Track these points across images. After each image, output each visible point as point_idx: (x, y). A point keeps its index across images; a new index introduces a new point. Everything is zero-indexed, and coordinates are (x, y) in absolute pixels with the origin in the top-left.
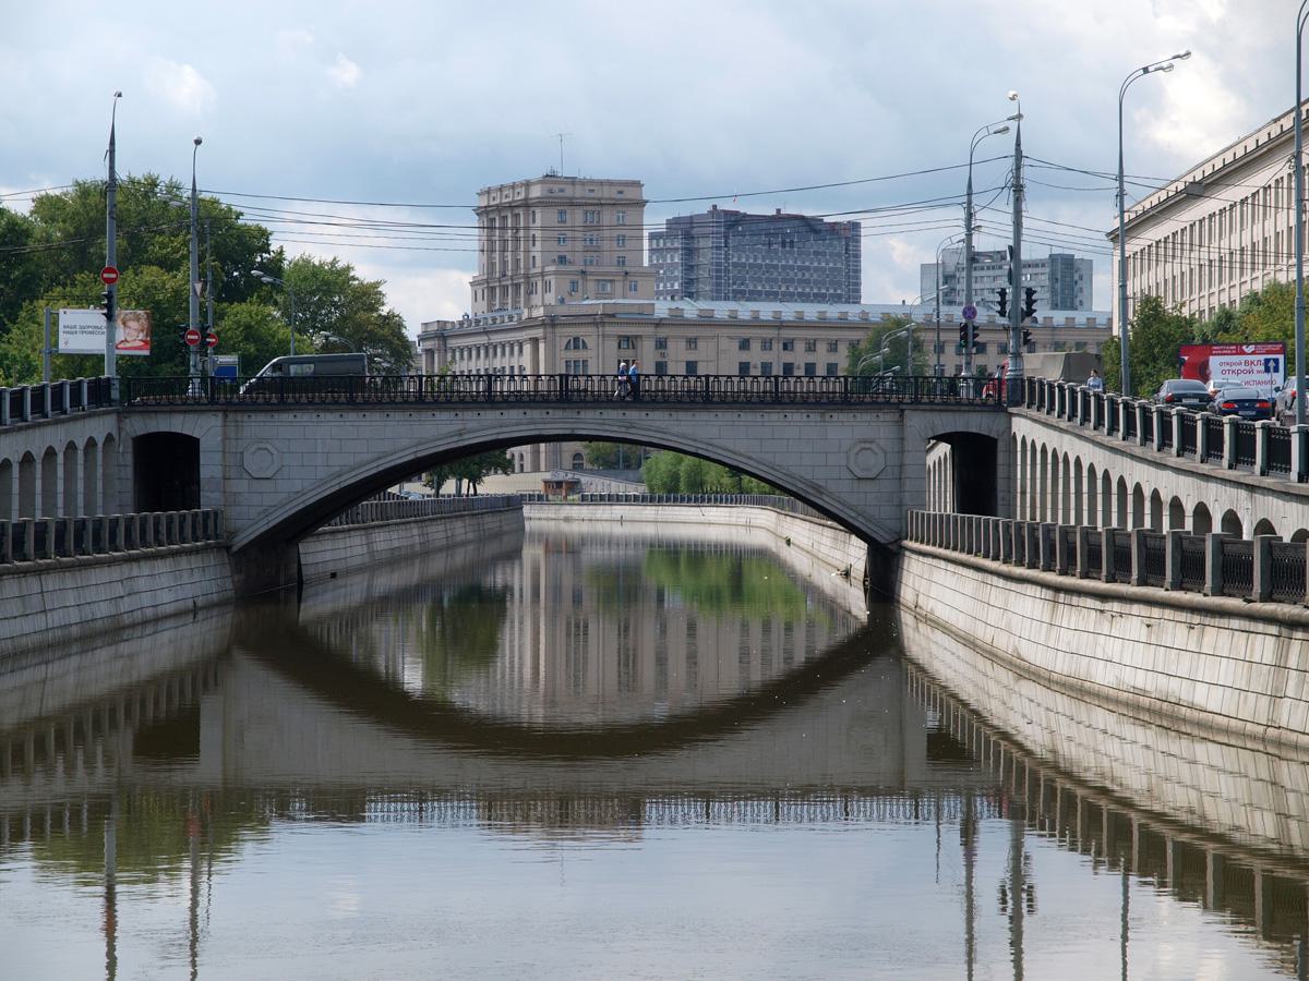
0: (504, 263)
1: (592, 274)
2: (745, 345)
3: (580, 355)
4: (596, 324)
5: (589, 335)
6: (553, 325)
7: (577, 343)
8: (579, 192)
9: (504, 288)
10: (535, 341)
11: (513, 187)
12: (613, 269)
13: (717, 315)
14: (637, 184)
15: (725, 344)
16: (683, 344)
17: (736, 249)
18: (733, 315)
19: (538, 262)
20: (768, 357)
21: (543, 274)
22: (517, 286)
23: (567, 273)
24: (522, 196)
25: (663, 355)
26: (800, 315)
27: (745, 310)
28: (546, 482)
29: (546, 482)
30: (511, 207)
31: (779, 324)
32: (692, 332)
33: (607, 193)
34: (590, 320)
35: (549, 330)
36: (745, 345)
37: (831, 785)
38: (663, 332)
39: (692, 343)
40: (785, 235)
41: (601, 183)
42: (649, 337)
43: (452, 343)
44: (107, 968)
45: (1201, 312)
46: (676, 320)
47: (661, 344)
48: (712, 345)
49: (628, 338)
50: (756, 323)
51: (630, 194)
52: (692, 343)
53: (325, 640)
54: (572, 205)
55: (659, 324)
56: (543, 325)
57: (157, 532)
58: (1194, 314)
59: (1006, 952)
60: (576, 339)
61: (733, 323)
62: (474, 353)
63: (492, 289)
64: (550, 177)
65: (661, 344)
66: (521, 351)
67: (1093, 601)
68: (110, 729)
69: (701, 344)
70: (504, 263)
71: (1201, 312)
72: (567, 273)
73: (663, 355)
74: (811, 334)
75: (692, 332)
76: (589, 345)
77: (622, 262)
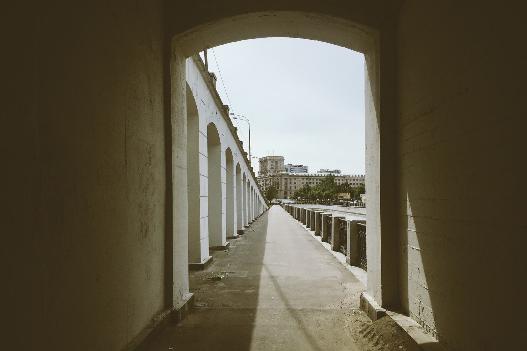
0: (263, 169)
1: (277, 170)
3: (278, 181)
4: (280, 176)
5: (279, 178)
6: (274, 176)
7: (277, 179)
8: (275, 158)
11: (265, 157)
13: (299, 175)
14: (283, 157)
16: (294, 179)
19: (268, 169)
20: (307, 181)
21: (269, 170)
23: (273, 170)
24: (266, 159)
30: (264, 161)
32: (295, 177)
34: (279, 176)
36: (303, 179)
38: (291, 177)
39: (295, 179)
41: (278, 157)
42: (289, 178)
44: (236, 129)
46: (293, 175)
47: (290, 179)
48: (298, 179)
51: (282, 158)
52: (295, 179)
55: (290, 176)
56: (272, 176)
59: (412, 327)
60: (277, 179)
63: (261, 173)
64: (269, 156)
65: (290, 179)
67: (408, 212)
68: (284, 178)
70: (263, 169)
72: (273, 170)
74: (313, 178)
75: (295, 177)
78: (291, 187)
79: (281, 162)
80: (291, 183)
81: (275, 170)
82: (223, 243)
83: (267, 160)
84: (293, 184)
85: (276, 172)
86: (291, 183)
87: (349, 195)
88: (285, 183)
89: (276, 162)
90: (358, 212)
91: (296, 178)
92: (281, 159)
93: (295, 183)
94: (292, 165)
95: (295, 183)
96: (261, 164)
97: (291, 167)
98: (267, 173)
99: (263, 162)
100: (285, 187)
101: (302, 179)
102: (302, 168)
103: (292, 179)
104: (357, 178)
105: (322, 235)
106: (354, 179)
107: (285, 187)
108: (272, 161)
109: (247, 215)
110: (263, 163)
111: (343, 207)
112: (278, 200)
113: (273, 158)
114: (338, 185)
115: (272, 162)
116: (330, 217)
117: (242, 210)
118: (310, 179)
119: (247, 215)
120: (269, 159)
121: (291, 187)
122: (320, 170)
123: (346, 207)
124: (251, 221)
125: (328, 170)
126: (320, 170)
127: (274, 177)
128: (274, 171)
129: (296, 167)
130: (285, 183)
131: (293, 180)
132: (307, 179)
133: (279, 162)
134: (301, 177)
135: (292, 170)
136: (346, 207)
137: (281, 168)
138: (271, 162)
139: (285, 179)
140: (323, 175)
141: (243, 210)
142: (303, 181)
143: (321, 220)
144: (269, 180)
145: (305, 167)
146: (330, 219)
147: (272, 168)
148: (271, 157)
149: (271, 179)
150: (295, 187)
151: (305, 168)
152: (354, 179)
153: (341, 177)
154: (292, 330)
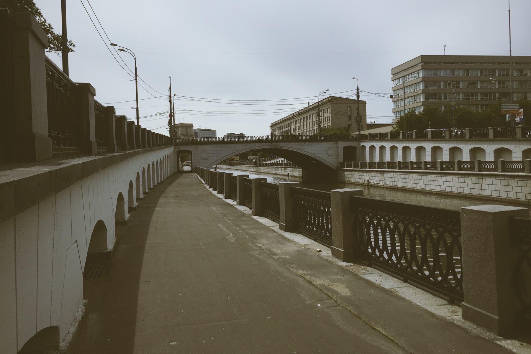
14: (192, 124)
51: (191, 125)
79: (190, 129)
81: (186, 136)
82: (141, 196)
83: (184, 126)
87: (238, 158)
89: (187, 129)
90: (236, 168)
92: (191, 126)
94: (201, 130)
97: (201, 131)
102: (211, 132)
105: (283, 215)
108: (183, 128)
109: (159, 174)
111: (250, 166)
112: (188, 162)
115: (183, 129)
117: (140, 186)
119: (159, 174)
120: (180, 126)
122: (227, 133)
123: (264, 167)
124: (162, 179)
125: (234, 133)
126: (227, 133)
129: (205, 131)
133: (189, 128)
135: (201, 133)
136: (264, 167)
137: (191, 134)
138: (182, 128)
141: (140, 184)
143: (223, 180)
145: (213, 131)
146: (217, 175)
147: (183, 134)
151: (213, 132)
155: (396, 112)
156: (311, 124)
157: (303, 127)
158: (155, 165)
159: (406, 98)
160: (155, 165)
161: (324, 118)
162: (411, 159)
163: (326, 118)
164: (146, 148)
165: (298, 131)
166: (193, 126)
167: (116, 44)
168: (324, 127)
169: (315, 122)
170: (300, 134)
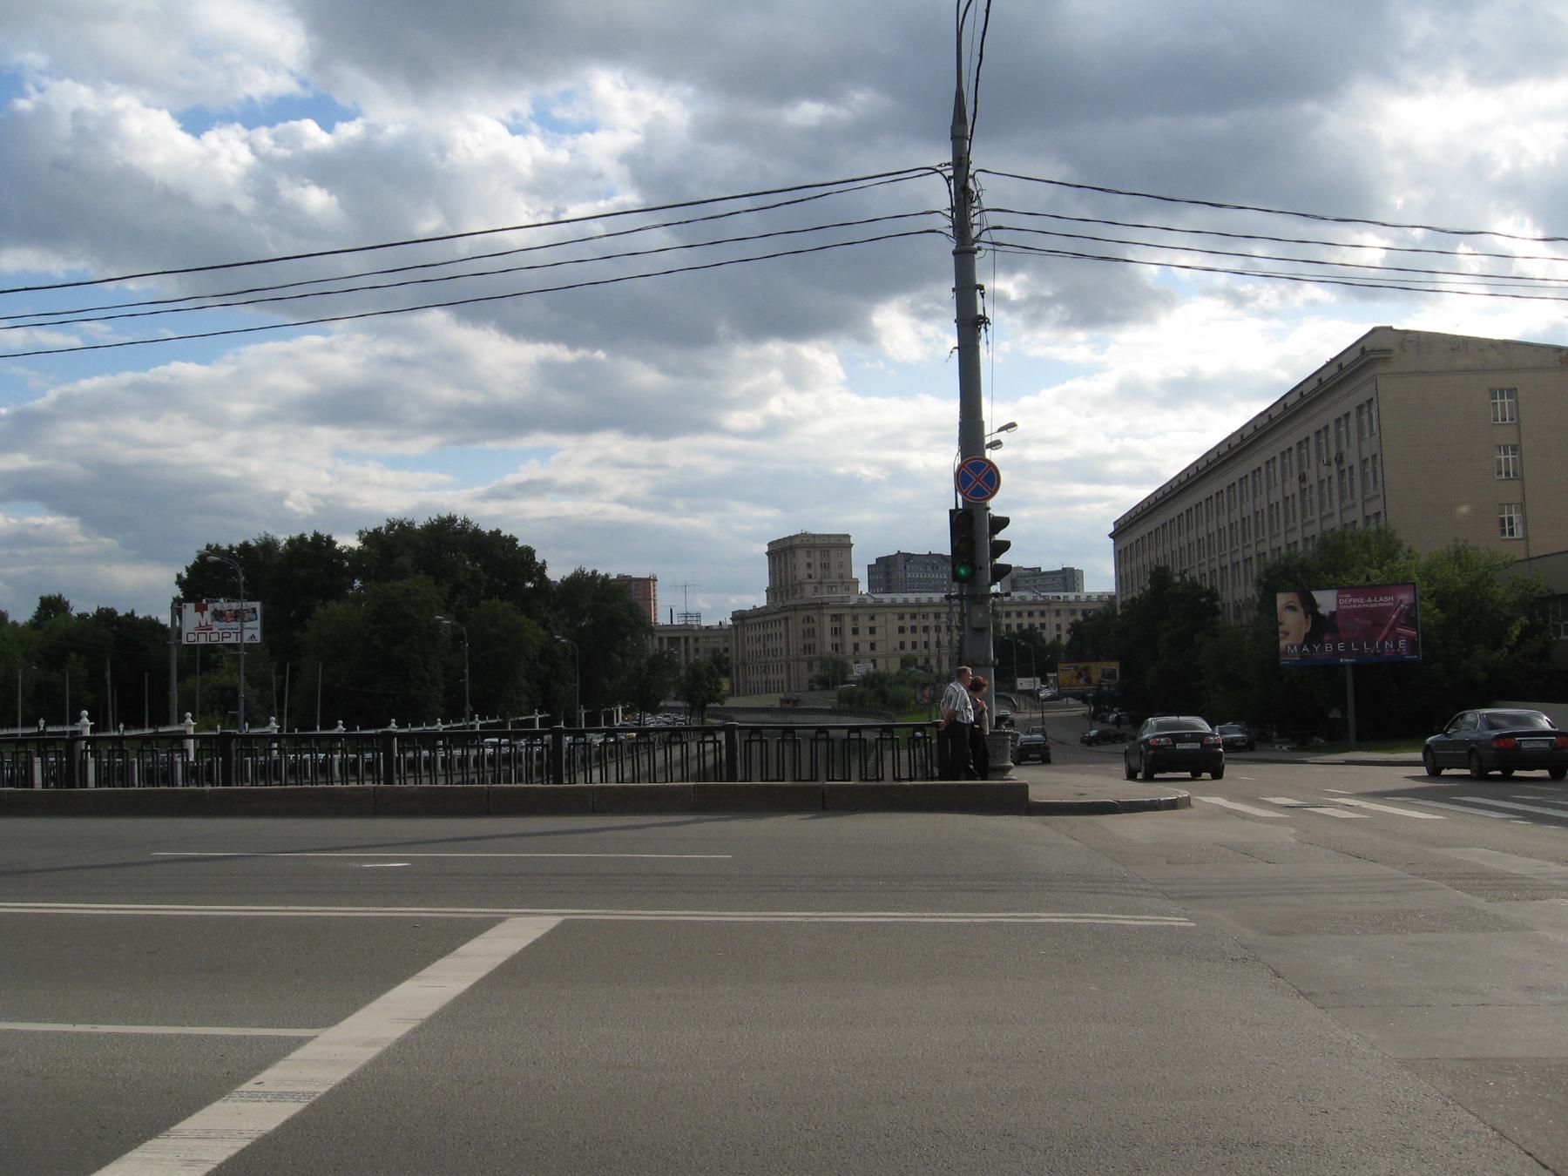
2: (901, 617)
9: (782, 593)
10: (787, 619)
12: (836, 581)
14: (848, 536)
15: (889, 617)
16: (867, 618)
17: (911, 571)
18: (893, 601)
22: (787, 591)
25: (856, 624)
26: (906, 600)
27: (900, 598)
28: (781, 700)
29: (781, 700)
31: (919, 605)
33: (833, 541)
35: (793, 612)
36: (901, 617)
37: (1079, 676)
38: (856, 611)
40: (934, 564)
43: (747, 621)
45: (1203, 575)
47: (855, 618)
49: (835, 616)
50: (906, 604)
51: (844, 541)
53: (1171, 570)
54: (814, 547)
55: (853, 607)
57: (751, 691)
58: (664, 653)
60: (808, 617)
61: (893, 605)
62: (769, 625)
65: (855, 618)
66: (780, 624)
69: (877, 618)
70: (781, 580)
71: (1203, 575)
73: (856, 624)
75: (872, 611)
76: (815, 618)
77: (841, 576)
78: (856, 647)
80: (855, 631)
83: (814, 546)
84: (864, 636)
85: (825, 589)
86: (855, 631)
88: (836, 632)
91: (857, 615)
93: (872, 631)
95: (872, 631)
96: (775, 562)
98: (794, 594)
99: (780, 557)
100: (836, 645)
101: (896, 617)
103: (860, 618)
104: (1083, 607)
106: (911, 614)
107: (836, 645)
108: (808, 552)
110: (781, 560)
113: (812, 542)
114: (1232, 623)
116: (144, 721)
118: (925, 616)
121: (856, 647)
127: (825, 611)
128: (815, 588)
130: (836, 632)
131: (864, 623)
132: (913, 616)
133: (833, 553)
134: (893, 610)
139: (836, 617)
140: (934, 601)
142: (901, 623)
144: (783, 623)
148: (805, 539)
149: (787, 619)
150: (873, 646)
152: (911, 614)
153: (905, 607)
154: (1139, 1009)
155: (1511, 504)
156: (1330, 490)
157: (1252, 532)
158: (718, 766)
159: (820, 740)
160: (718, 766)
161: (1341, 473)
162: (1033, 310)
163: (1357, 470)
164: (668, 638)
165: (1244, 548)
166: (852, 545)
167: (1012, 421)
168: (1324, 533)
169: (1281, 505)
170: (1300, 544)
